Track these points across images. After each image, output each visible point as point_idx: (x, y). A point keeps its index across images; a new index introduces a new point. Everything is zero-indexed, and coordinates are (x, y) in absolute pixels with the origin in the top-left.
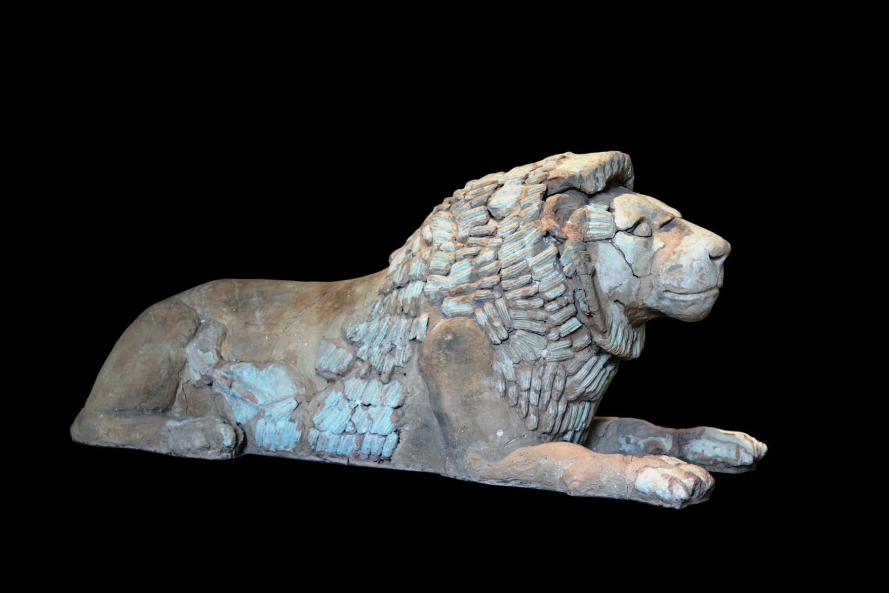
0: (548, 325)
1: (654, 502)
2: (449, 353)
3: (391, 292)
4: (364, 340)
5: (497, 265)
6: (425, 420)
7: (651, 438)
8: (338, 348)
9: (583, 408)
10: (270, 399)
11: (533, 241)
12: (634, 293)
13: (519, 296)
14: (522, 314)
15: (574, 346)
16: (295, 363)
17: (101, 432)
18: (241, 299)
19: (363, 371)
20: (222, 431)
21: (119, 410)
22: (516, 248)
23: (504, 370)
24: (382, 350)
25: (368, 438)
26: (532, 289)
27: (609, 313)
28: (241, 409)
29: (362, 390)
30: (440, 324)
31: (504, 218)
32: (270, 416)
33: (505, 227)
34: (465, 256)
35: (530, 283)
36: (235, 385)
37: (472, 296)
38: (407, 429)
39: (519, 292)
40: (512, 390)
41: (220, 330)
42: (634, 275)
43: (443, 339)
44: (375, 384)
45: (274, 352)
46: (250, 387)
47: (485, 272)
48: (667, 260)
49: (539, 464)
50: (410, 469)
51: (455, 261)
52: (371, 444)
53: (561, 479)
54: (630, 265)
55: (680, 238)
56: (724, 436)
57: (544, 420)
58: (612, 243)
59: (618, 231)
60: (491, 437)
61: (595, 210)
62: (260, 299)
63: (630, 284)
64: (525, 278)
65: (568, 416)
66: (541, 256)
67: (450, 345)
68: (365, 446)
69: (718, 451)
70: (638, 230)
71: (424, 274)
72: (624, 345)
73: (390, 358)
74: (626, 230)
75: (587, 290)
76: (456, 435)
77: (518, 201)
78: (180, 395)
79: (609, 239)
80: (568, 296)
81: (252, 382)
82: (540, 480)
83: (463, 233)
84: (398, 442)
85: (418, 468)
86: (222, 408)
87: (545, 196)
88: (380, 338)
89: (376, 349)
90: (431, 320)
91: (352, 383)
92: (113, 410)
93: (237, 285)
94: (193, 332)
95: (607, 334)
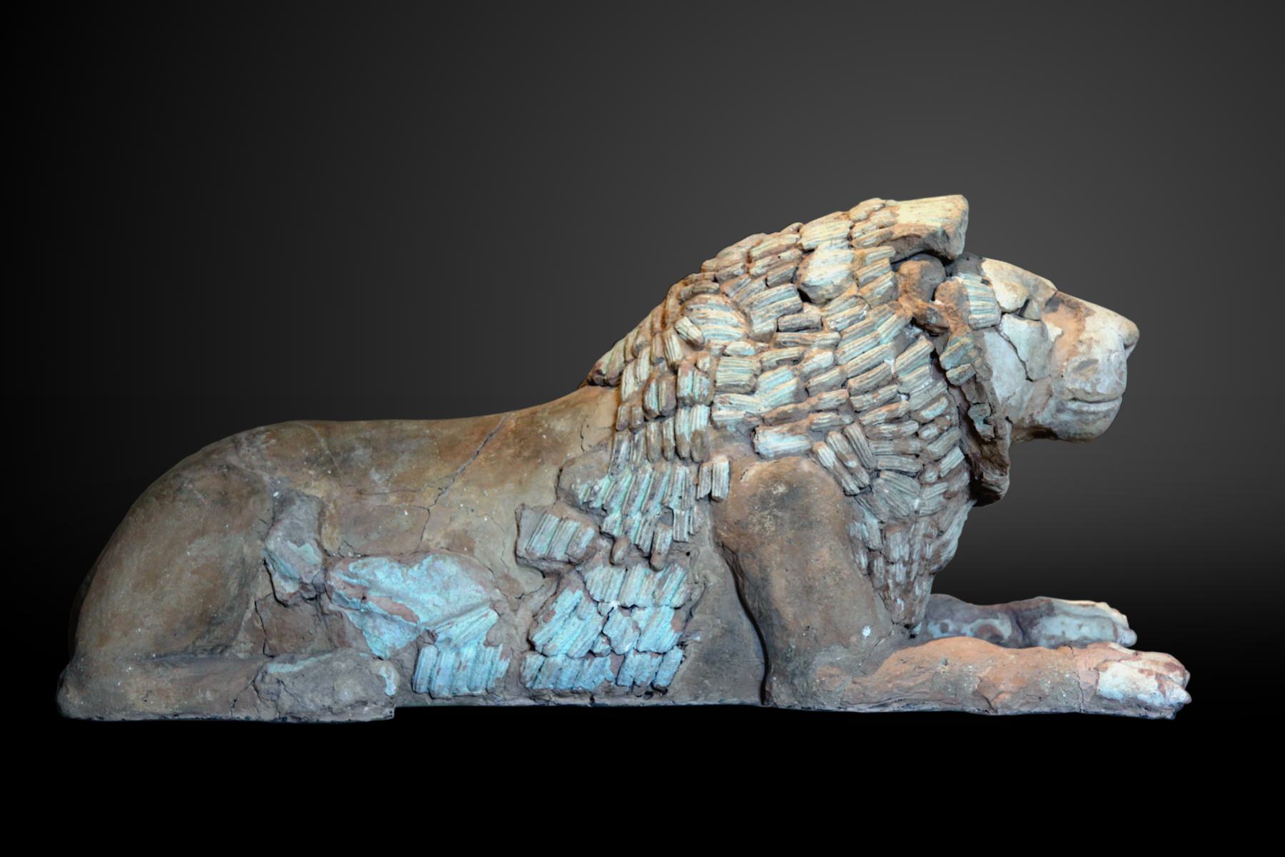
1: (1129, 713)
2: (780, 514)
4: (613, 505)
5: (842, 372)
6: (728, 623)
7: (980, 622)
10: (438, 613)
11: (893, 334)
13: (881, 419)
14: (888, 447)
16: (471, 550)
17: (133, 696)
21: (159, 656)
22: (869, 343)
24: (650, 517)
25: (634, 660)
26: (902, 406)
28: (381, 634)
29: (618, 585)
30: (754, 470)
33: (839, 314)
34: (780, 363)
36: (372, 594)
37: (805, 423)
38: (698, 639)
39: (883, 413)
40: (879, 563)
41: (314, 507)
42: (1028, 379)
43: (769, 493)
45: (426, 536)
46: (398, 596)
47: (822, 384)
48: (1074, 352)
49: (937, 673)
50: (700, 702)
51: (763, 371)
53: (975, 693)
54: (1023, 363)
55: (1081, 320)
56: (1082, 609)
59: (1003, 313)
60: (854, 639)
62: (369, 451)
63: (1023, 393)
64: (885, 393)
66: (909, 355)
67: (782, 501)
68: (628, 675)
71: (706, 393)
73: (665, 529)
77: (853, 276)
78: (251, 620)
79: (995, 327)
81: (396, 588)
82: (939, 696)
83: (763, 326)
85: (714, 700)
89: (636, 517)
91: (598, 574)
92: (148, 656)
93: (316, 431)
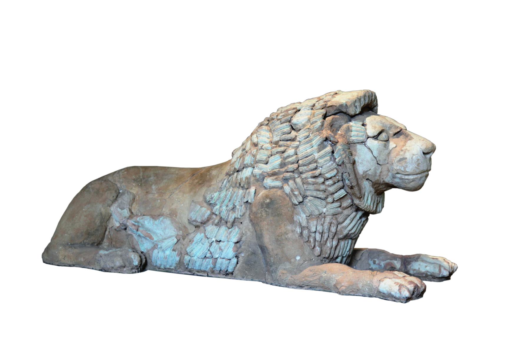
0: (326, 194)
2: (268, 210)
3: (233, 174)
4: (217, 203)
5: (297, 158)
6: (254, 250)
7: (388, 261)
8: (201, 207)
9: (348, 243)
10: (161, 238)
11: (318, 143)
12: (378, 175)
13: (309, 176)
14: (311, 187)
15: (342, 206)
16: (176, 216)
17: (60, 257)
18: (144, 178)
19: (216, 221)
20: (132, 257)
21: (71, 244)
23: (301, 220)
24: (228, 208)
25: (219, 260)
26: (317, 172)
27: (363, 186)
28: (144, 243)
29: (216, 232)
30: (262, 193)
31: (300, 130)
32: (161, 247)
33: (301, 135)
34: (277, 153)
35: (316, 169)
36: (140, 229)
37: (282, 176)
38: (243, 255)
39: (310, 174)
40: (305, 232)
41: (131, 196)
42: (378, 164)
43: (264, 202)
44: (223, 228)
45: (164, 210)
46: (149, 230)
47: (289, 162)
48: (398, 154)
49: (322, 276)
51: (272, 155)
52: (221, 265)
54: (375, 158)
55: (406, 142)
57: (324, 250)
58: (365, 145)
59: (368, 138)
60: (293, 260)
61: (355, 125)
62: (155, 178)
63: (375, 169)
64: (313, 166)
65: (338, 247)
66: (323, 152)
67: (268, 205)
68: (218, 266)
69: (428, 269)
70: (380, 137)
71: (252, 163)
72: (372, 205)
73: (232, 213)
74: (373, 137)
75: (350, 172)
76: (272, 259)
77: (309, 120)
78: (107, 235)
79: (363, 142)
80: (338, 176)
81: (150, 227)
82: (322, 285)
83: (276, 139)
84: (237, 263)
86: (132, 243)
87: (325, 117)
88: (226, 201)
89: (224, 208)
90: (257, 190)
91: (210, 228)
92: (67, 244)
94: (115, 197)
95: (362, 199)
